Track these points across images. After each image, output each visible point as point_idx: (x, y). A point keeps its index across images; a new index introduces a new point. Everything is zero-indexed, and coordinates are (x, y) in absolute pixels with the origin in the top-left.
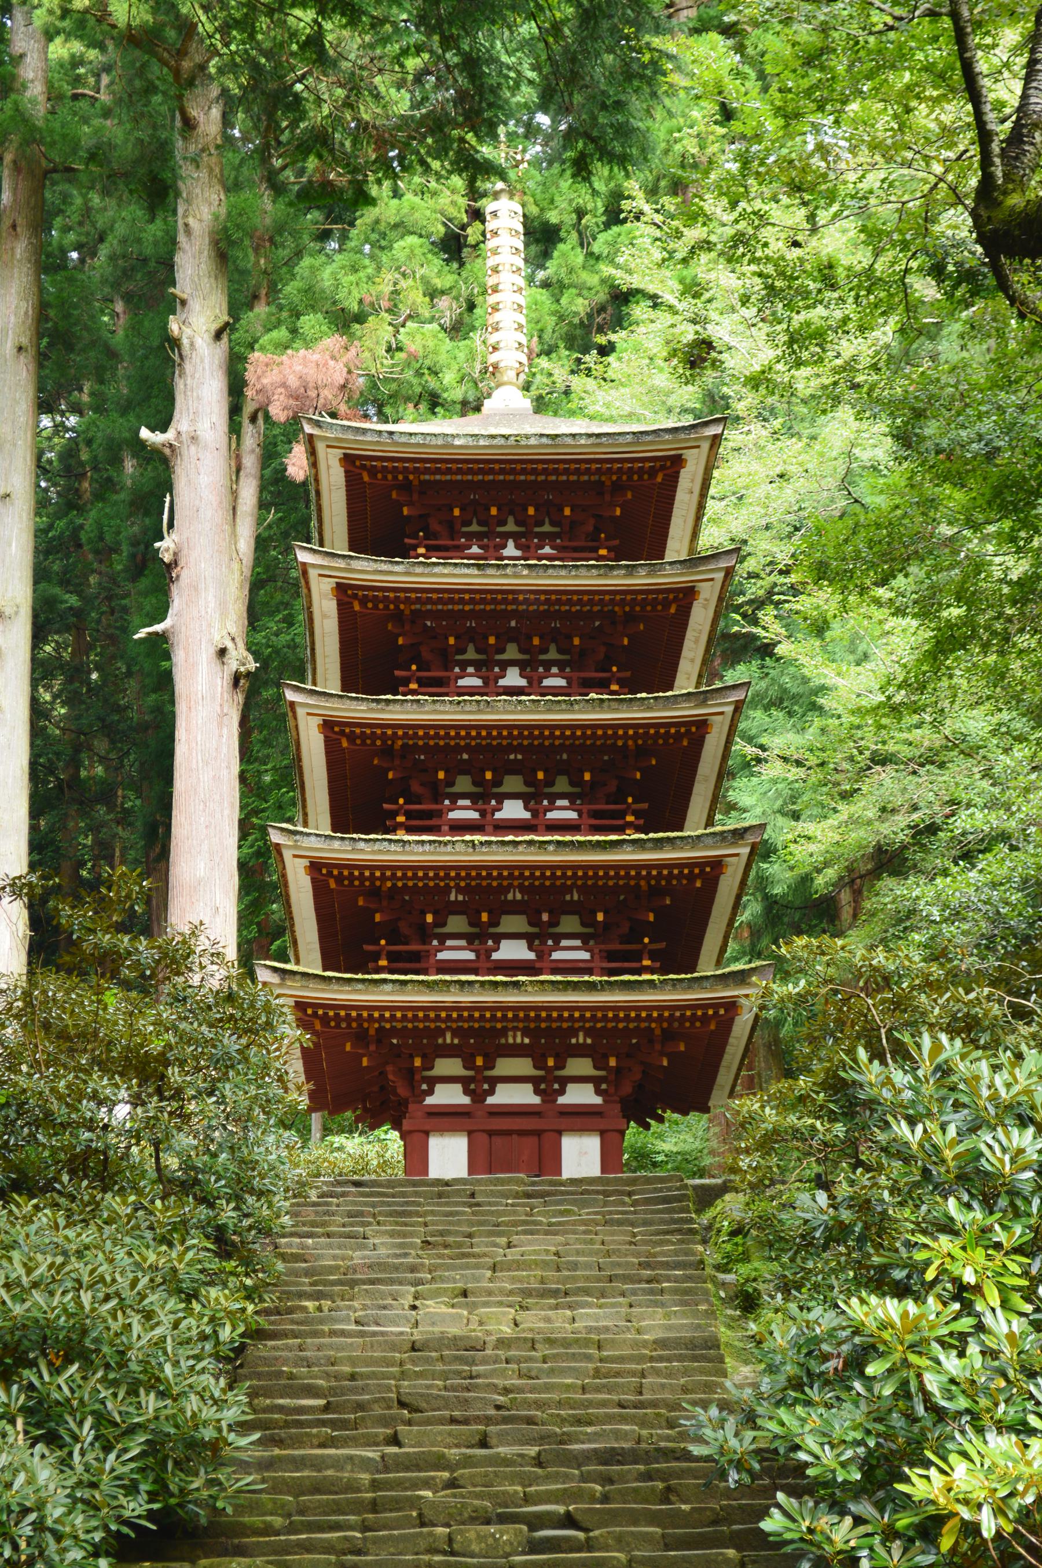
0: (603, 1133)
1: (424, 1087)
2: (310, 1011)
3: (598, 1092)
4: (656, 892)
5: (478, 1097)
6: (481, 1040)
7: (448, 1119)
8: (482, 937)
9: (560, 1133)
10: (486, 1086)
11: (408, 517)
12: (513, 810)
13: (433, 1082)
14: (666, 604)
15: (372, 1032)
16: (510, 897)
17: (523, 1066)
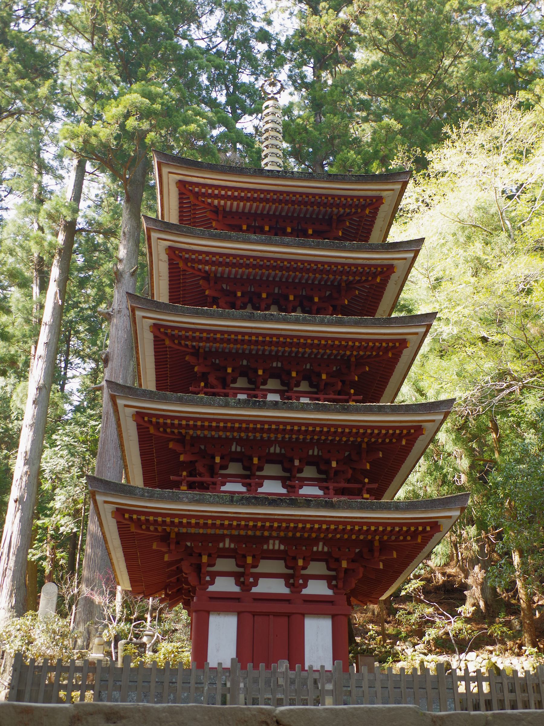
0: (334, 617)
1: (208, 578)
2: (127, 516)
3: (330, 587)
4: (372, 448)
5: (245, 586)
6: (248, 545)
7: (224, 603)
8: (251, 478)
9: (303, 615)
10: (251, 580)
11: (183, 462)
12: (272, 487)
13: (214, 575)
14: (400, 437)
15: (173, 536)
16: (272, 450)
17: (278, 566)
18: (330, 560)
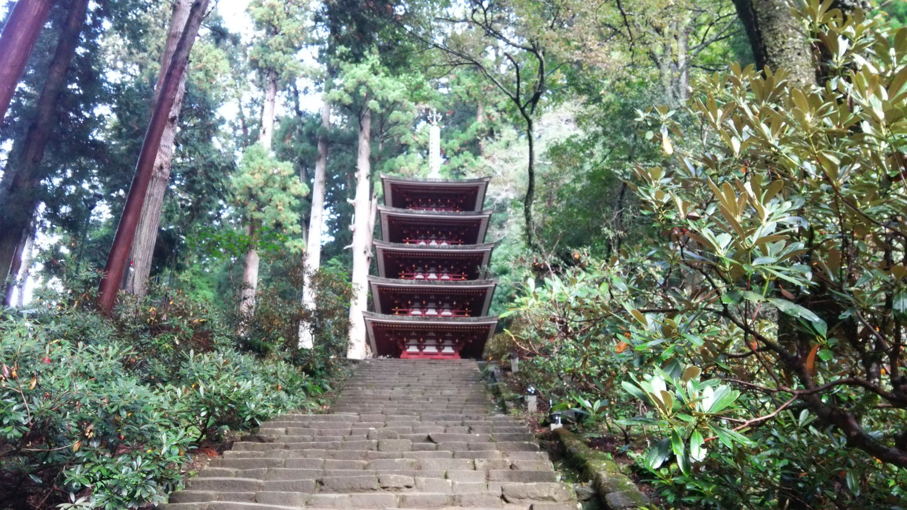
5: (421, 350)
18: (453, 339)
